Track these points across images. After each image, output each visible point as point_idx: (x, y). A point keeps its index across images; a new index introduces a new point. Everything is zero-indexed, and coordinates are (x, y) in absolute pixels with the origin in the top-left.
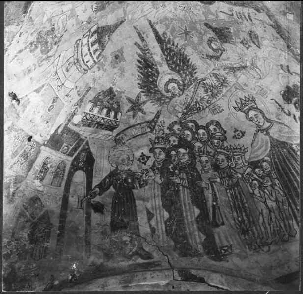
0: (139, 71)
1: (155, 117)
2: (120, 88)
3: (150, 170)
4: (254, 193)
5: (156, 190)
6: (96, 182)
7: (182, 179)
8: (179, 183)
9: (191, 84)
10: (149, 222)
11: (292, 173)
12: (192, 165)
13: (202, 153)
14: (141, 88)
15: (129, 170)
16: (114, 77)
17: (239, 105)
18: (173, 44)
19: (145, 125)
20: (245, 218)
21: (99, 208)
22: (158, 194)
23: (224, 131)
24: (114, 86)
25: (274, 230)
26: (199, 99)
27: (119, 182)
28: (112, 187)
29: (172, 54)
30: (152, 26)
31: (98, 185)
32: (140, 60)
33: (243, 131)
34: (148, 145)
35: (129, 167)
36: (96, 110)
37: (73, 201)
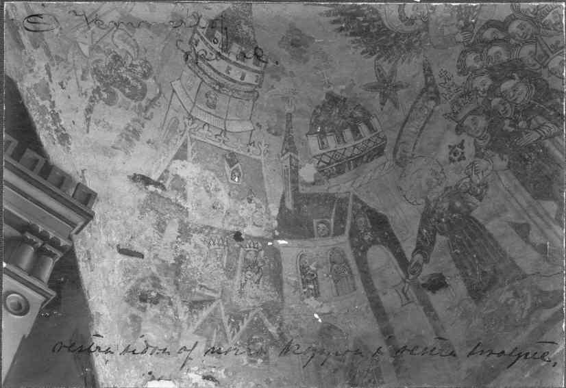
0: (346, 35)
1: (426, 76)
2: (344, 84)
3: (477, 159)
6: (408, 247)
7: (540, 126)
8: (540, 138)
10: (527, 242)
14: (372, 54)
15: (446, 189)
16: (319, 75)
19: (420, 102)
21: (438, 283)
27: (443, 220)
31: (416, 250)
34: (449, 127)
36: (331, 142)
37: (390, 300)
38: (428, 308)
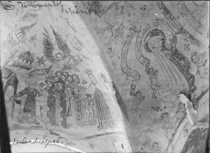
0: (44, 46)
4: (85, 106)
5: (45, 99)
6: (18, 91)
7: (58, 96)
9: (68, 57)
10: (40, 111)
11: (101, 102)
12: (63, 91)
13: (68, 87)
14: (44, 53)
15: (35, 88)
17: (87, 71)
18: (61, 38)
20: (80, 115)
21: (19, 102)
22: (46, 100)
23: (79, 79)
24: (31, 51)
25: (90, 121)
26: (70, 64)
27: (29, 93)
28: (26, 94)
29: (61, 41)
30: (51, 27)
32: (45, 41)
33: (87, 81)
34: (45, 79)
35: (34, 87)
36: (20, 60)
38: (13, 106)
